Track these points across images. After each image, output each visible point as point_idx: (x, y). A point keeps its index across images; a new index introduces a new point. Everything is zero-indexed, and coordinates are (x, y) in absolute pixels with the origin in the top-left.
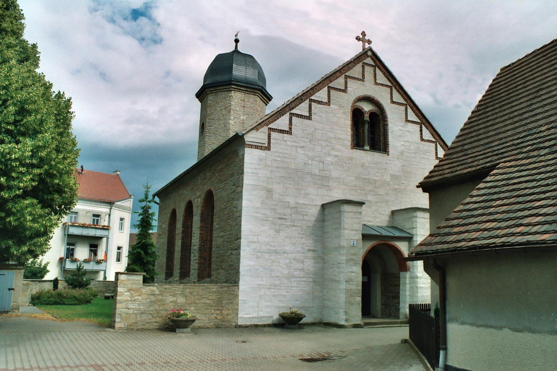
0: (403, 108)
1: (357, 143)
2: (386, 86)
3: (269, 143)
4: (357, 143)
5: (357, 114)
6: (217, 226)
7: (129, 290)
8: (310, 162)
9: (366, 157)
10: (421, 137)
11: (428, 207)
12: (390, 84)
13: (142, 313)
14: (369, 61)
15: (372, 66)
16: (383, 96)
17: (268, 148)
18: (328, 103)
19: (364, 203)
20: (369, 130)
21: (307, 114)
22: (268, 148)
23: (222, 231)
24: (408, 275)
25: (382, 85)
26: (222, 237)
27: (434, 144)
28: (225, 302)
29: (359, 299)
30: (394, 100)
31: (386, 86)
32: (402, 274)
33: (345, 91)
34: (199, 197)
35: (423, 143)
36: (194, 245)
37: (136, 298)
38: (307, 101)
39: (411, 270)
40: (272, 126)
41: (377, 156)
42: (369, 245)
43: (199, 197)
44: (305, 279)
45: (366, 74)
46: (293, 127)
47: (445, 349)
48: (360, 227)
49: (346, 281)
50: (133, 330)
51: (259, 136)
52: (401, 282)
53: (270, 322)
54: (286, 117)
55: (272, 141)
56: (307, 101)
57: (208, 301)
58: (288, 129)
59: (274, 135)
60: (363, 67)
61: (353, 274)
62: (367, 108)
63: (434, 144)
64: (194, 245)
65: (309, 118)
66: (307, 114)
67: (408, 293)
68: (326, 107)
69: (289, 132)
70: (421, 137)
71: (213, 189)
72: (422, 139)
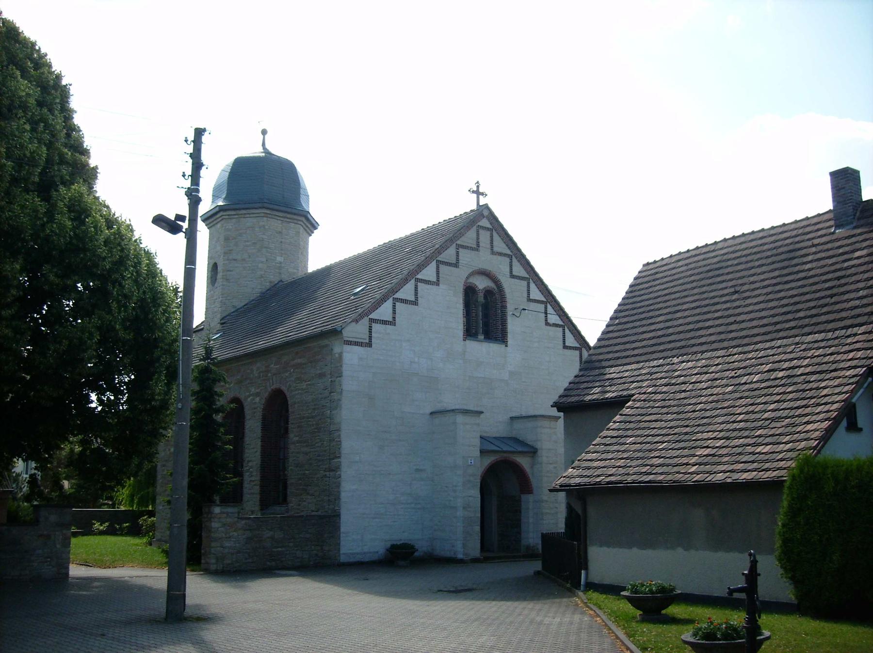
0: (525, 283)
1: (470, 333)
2: (505, 255)
3: (370, 337)
4: (470, 333)
5: (469, 292)
6: (297, 439)
7: (224, 525)
8: (416, 360)
9: (481, 349)
10: (546, 320)
11: (481, 204)
12: (509, 252)
13: (239, 552)
14: (484, 223)
15: (488, 229)
16: (500, 267)
17: (369, 344)
18: (437, 283)
19: (482, 412)
20: (485, 316)
21: (413, 299)
22: (369, 344)
23: (307, 446)
24: (531, 498)
25: (500, 254)
26: (306, 454)
27: (561, 329)
28: (326, 536)
29: (478, 528)
30: (514, 273)
31: (505, 255)
32: (524, 497)
33: (456, 265)
34: (257, 394)
35: (549, 327)
36: (249, 461)
37: (231, 534)
38: (413, 281)
39: (535, 491)
40: (373, 316)
41: (494, 348)
42: (488, 461)
43: (257, 394)
44: (413, 505)
45: (481, 239)
46: (397, 316)
47: (586, 569)
48: (477, 442)
49: (464, 508)
50: (402, 563)
51: (356, 331)
52: (523, 506)
53: (375, 557)
54: (389, 304)
55: (373, 335)
56: (413, 281)
57: (308, 536)
58: (391, 320)
59: (376, 327)
60: (478, 231)
61: (471, 499)
62: (482, 284)
63: (561, 329)
64: (249, 461)
65: (415, 303)
66: (413, 299)
67: (531, 520)
68: (434, 287)
69: (393, 323)
70: (546, 320)
71: (284, 388)
72: (547, 324)
